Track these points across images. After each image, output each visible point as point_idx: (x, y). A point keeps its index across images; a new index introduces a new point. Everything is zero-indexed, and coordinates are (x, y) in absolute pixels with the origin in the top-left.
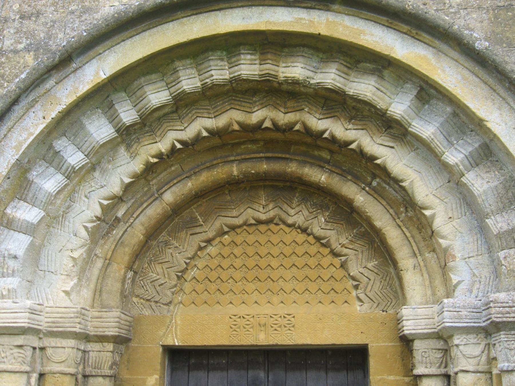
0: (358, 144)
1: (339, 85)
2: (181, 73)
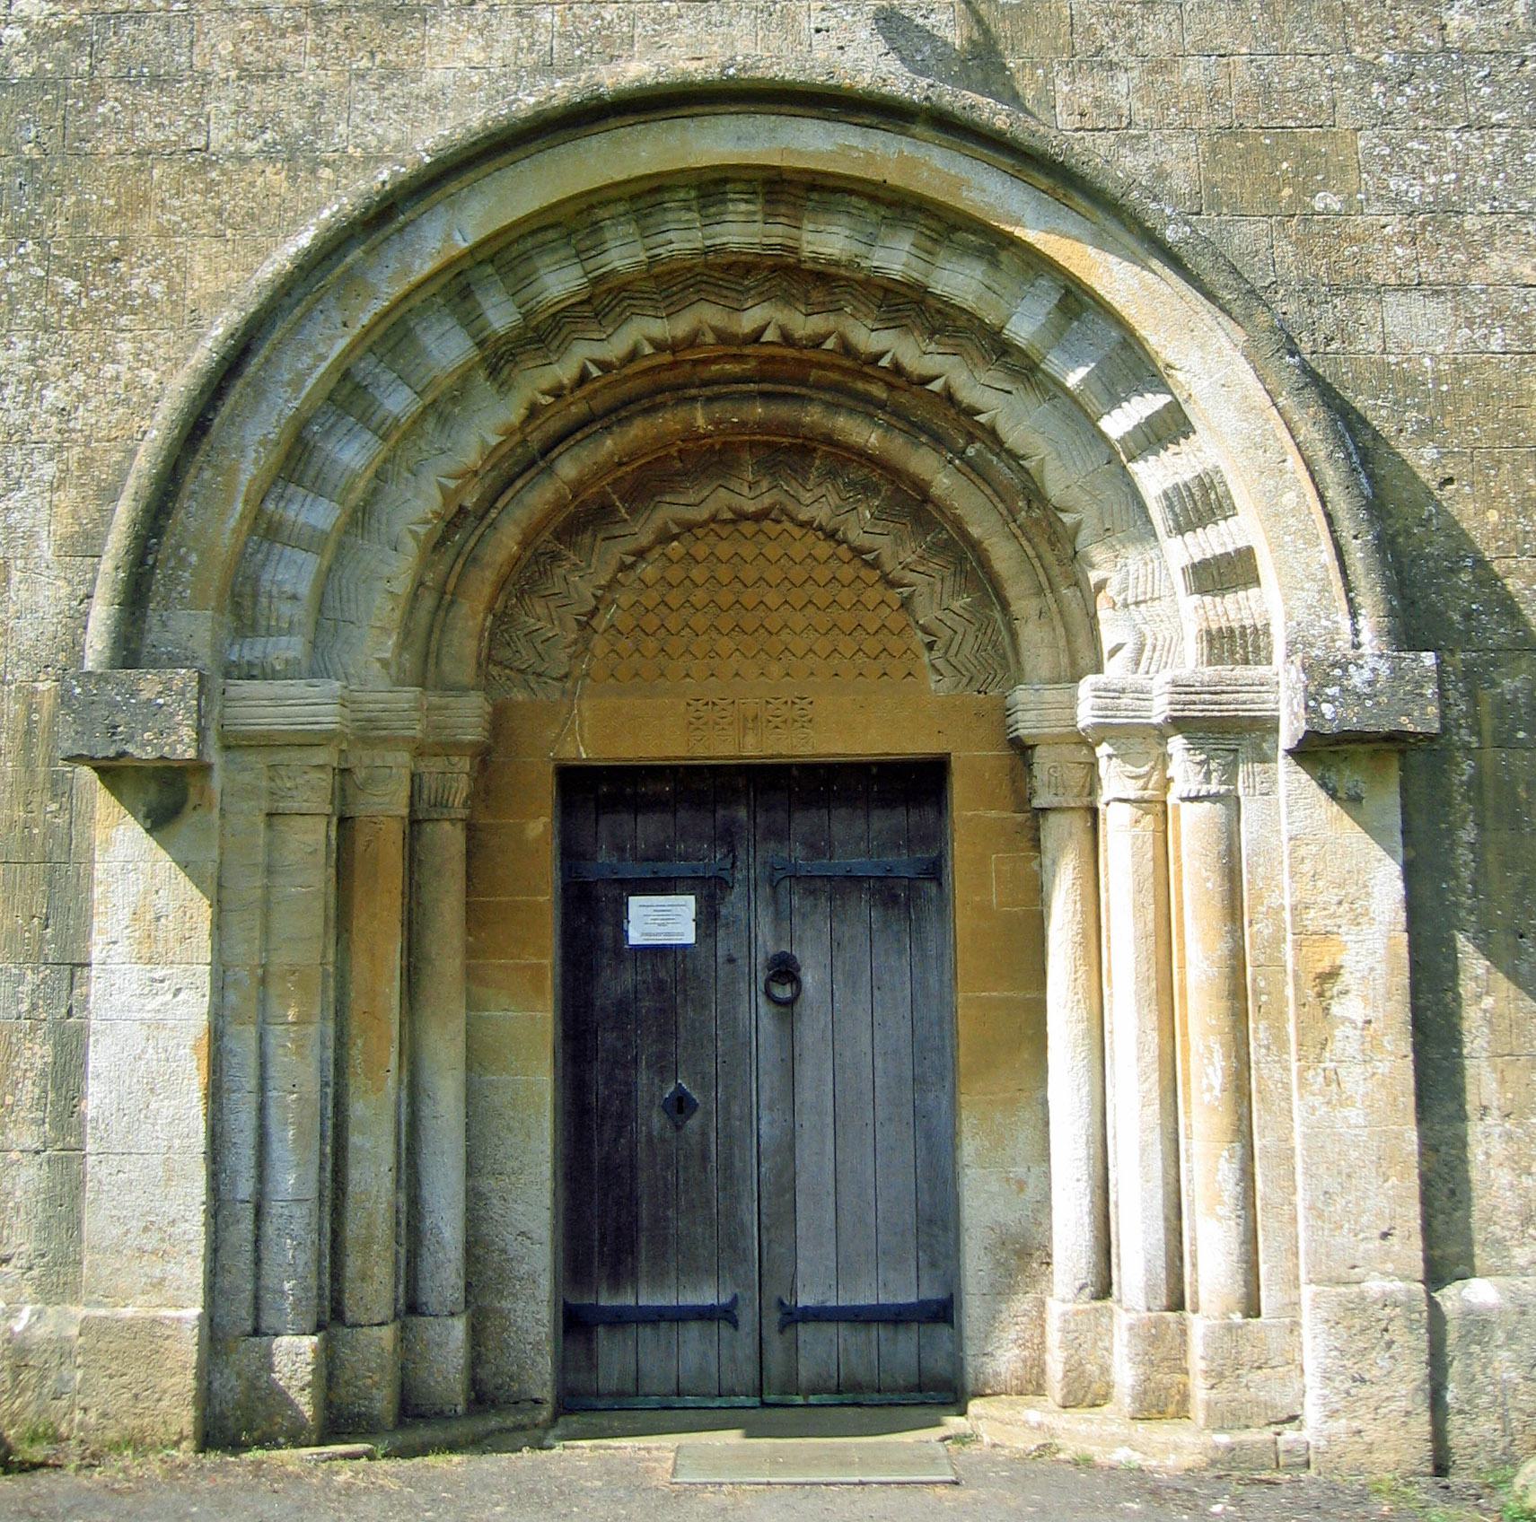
0: (946, 383)
1: (915, 275)
2: (608, 235)
